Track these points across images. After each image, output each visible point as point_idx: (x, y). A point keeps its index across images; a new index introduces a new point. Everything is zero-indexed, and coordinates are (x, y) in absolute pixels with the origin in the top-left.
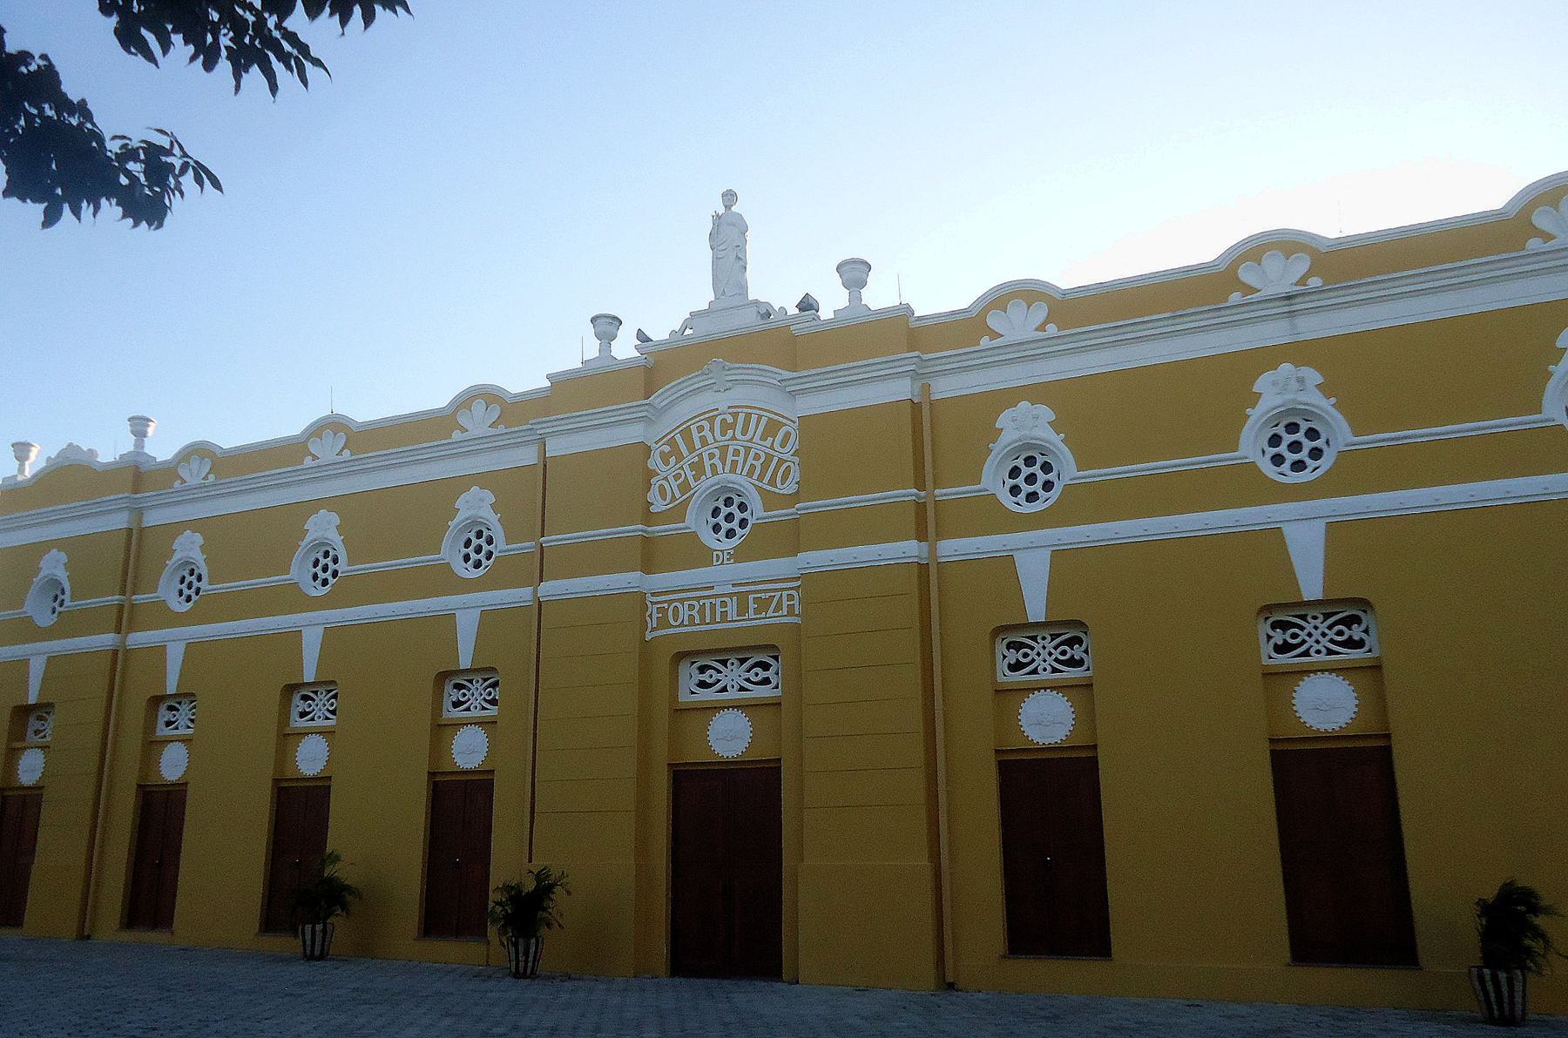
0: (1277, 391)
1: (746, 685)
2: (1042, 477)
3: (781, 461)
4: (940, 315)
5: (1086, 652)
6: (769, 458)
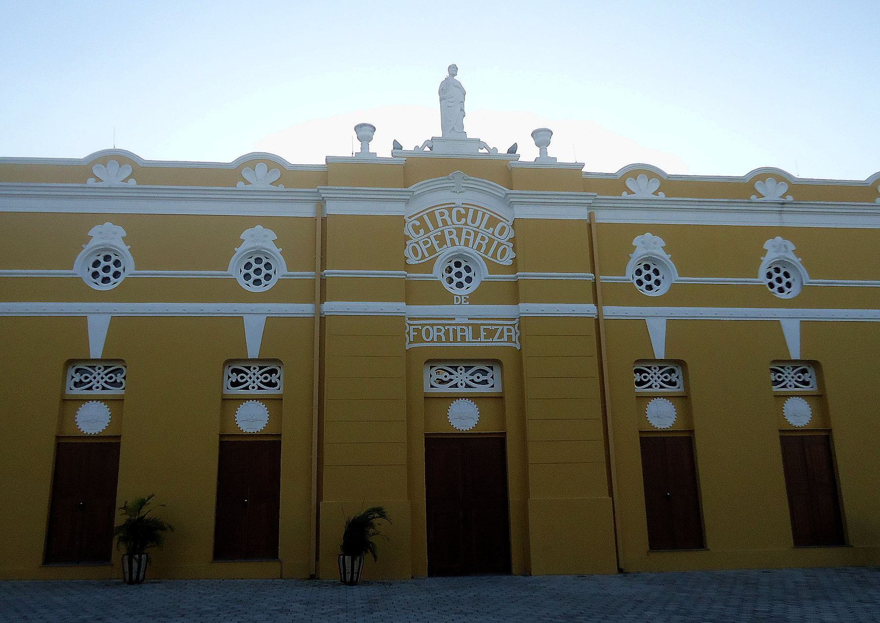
1: (262, 386)
3: (499, 244)
4: (307, 166)
5: (229, 377)
6: (491, 241)
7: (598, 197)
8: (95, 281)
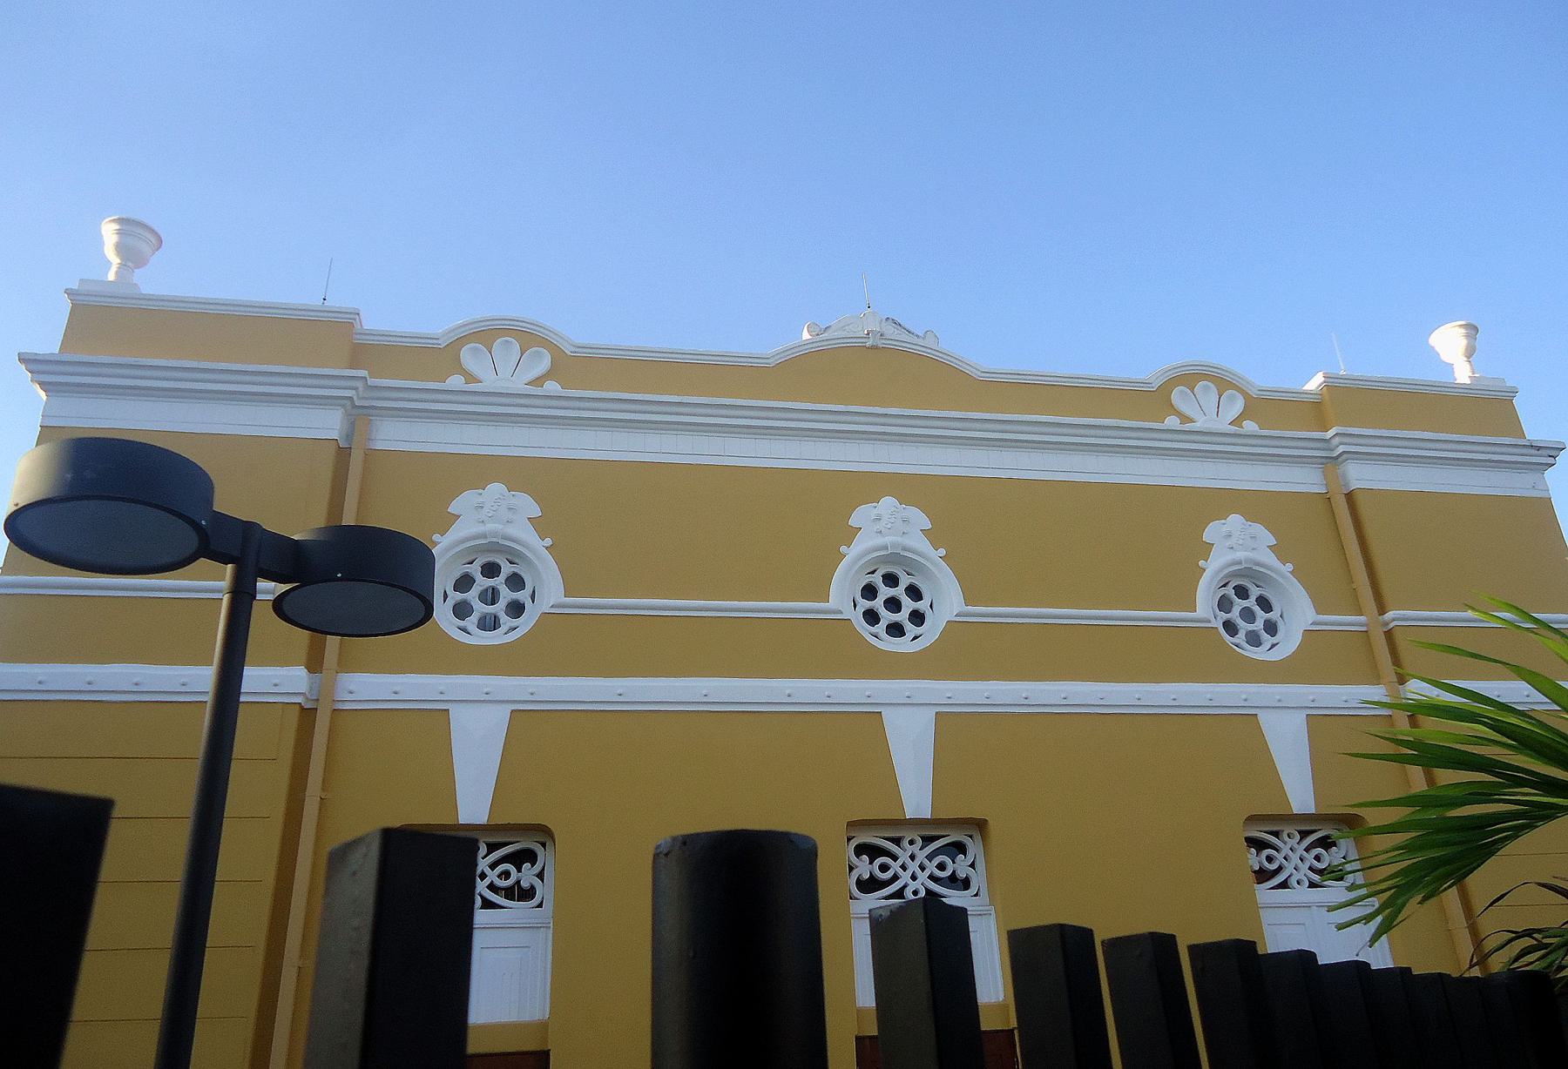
0: (1234, 543)
2: (506, 595)
5: (540, 876)
7: (371, 382)
8: (461, 623)
